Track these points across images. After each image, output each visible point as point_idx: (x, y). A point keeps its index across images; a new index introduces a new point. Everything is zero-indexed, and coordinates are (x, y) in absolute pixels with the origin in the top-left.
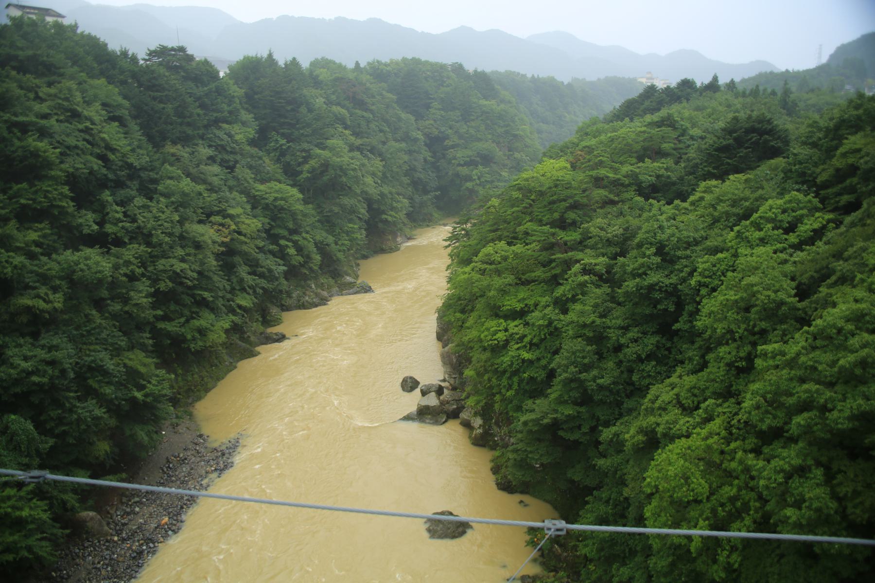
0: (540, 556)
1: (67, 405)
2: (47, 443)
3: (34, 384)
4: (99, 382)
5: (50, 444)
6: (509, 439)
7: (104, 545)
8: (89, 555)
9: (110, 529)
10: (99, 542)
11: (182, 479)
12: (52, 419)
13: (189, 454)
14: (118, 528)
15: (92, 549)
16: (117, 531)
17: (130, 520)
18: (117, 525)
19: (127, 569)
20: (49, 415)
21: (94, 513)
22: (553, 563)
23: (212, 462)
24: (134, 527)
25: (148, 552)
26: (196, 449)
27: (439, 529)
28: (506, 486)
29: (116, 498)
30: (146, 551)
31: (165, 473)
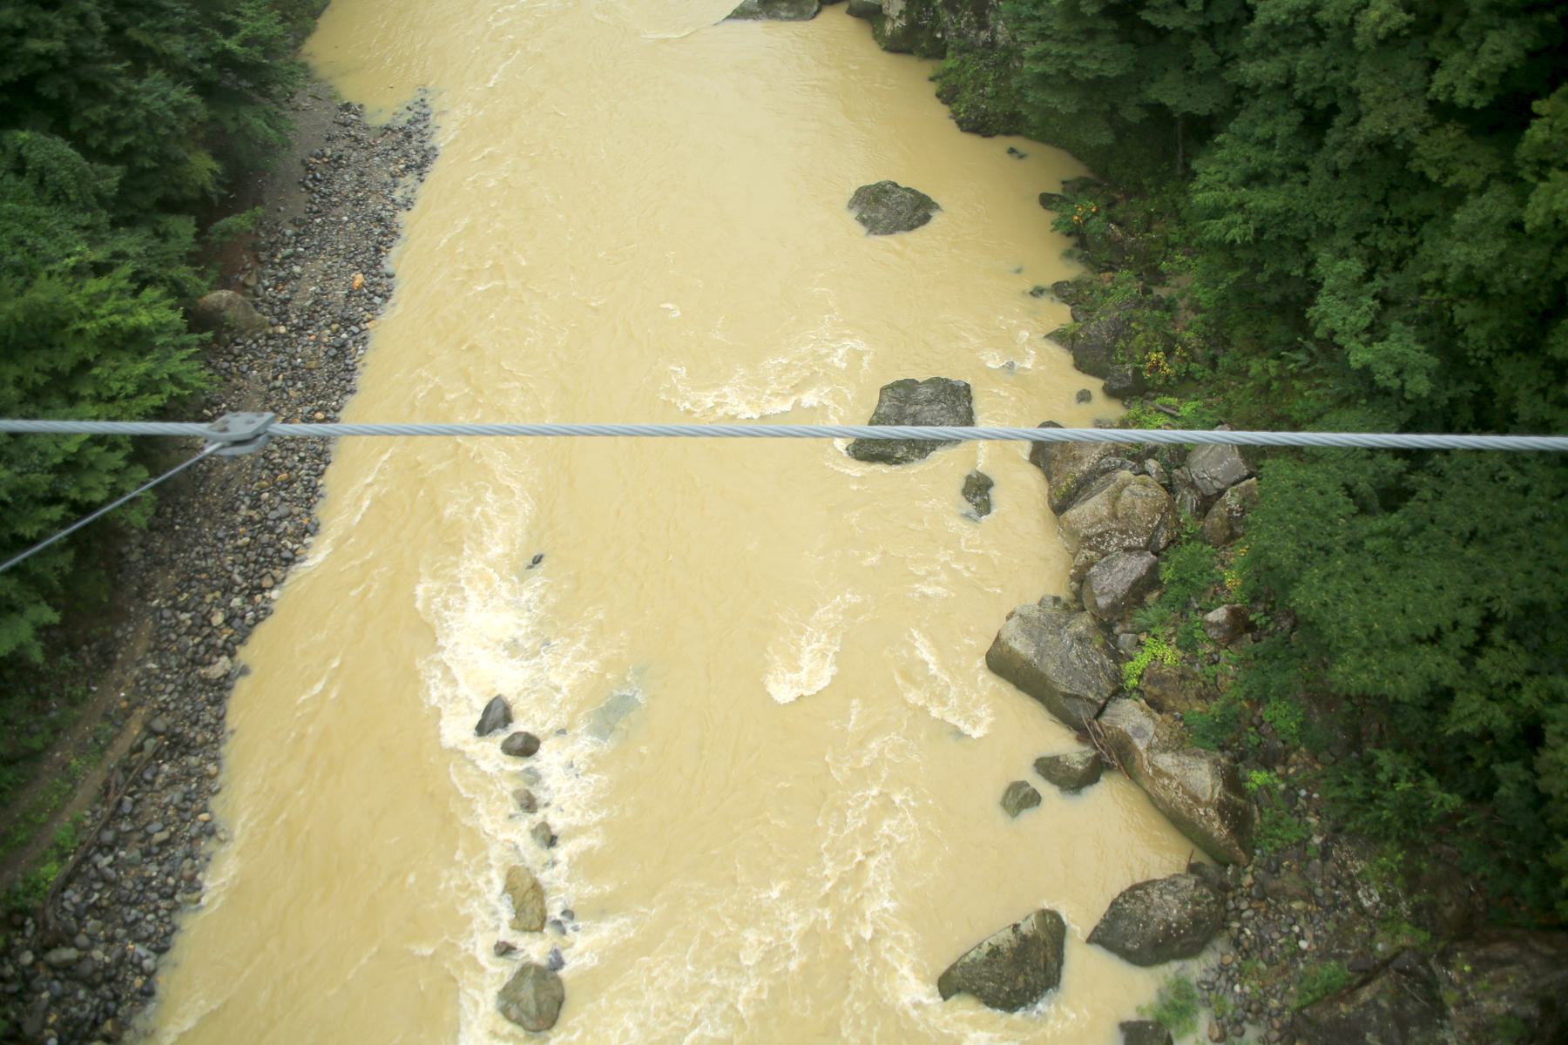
0: (1076, 245)
1: (118, 92)
2: (109, 176)
3: (39, 57)
4: (150, 30)
5: (117, 178)
6: (976, 35)
7: (267, 345)
8: (251, 368)
9: (264, 314)
10: (256, 341)
11: (351, 196)
12: (95, 126)
13: (341, 147)
14: (277, 310)
15: (250, 356)
16: (278, 316)
17: (292, 292)
18: (272, 304)
19: (331, 379)
20: (86, 119)
21: (231, 292)
22: (1105, 255)
23: (394, 155)
24: (308, 303)
25: (355, 342)
26: (350, 136)
27: (880, 216)
28: (977, 125)
29: (244, 257)
30: (351, 342)
31: (313, 191)
